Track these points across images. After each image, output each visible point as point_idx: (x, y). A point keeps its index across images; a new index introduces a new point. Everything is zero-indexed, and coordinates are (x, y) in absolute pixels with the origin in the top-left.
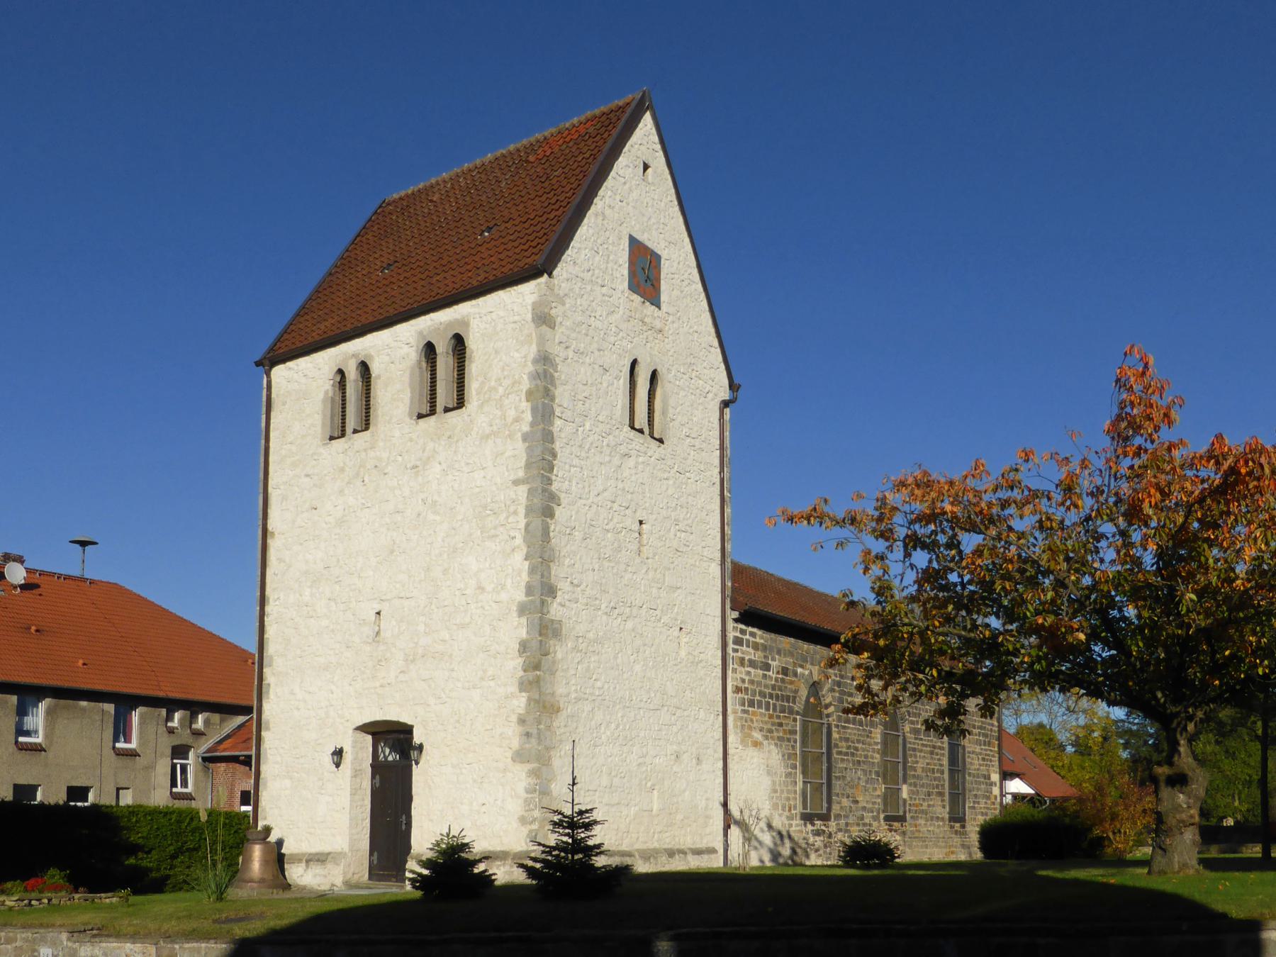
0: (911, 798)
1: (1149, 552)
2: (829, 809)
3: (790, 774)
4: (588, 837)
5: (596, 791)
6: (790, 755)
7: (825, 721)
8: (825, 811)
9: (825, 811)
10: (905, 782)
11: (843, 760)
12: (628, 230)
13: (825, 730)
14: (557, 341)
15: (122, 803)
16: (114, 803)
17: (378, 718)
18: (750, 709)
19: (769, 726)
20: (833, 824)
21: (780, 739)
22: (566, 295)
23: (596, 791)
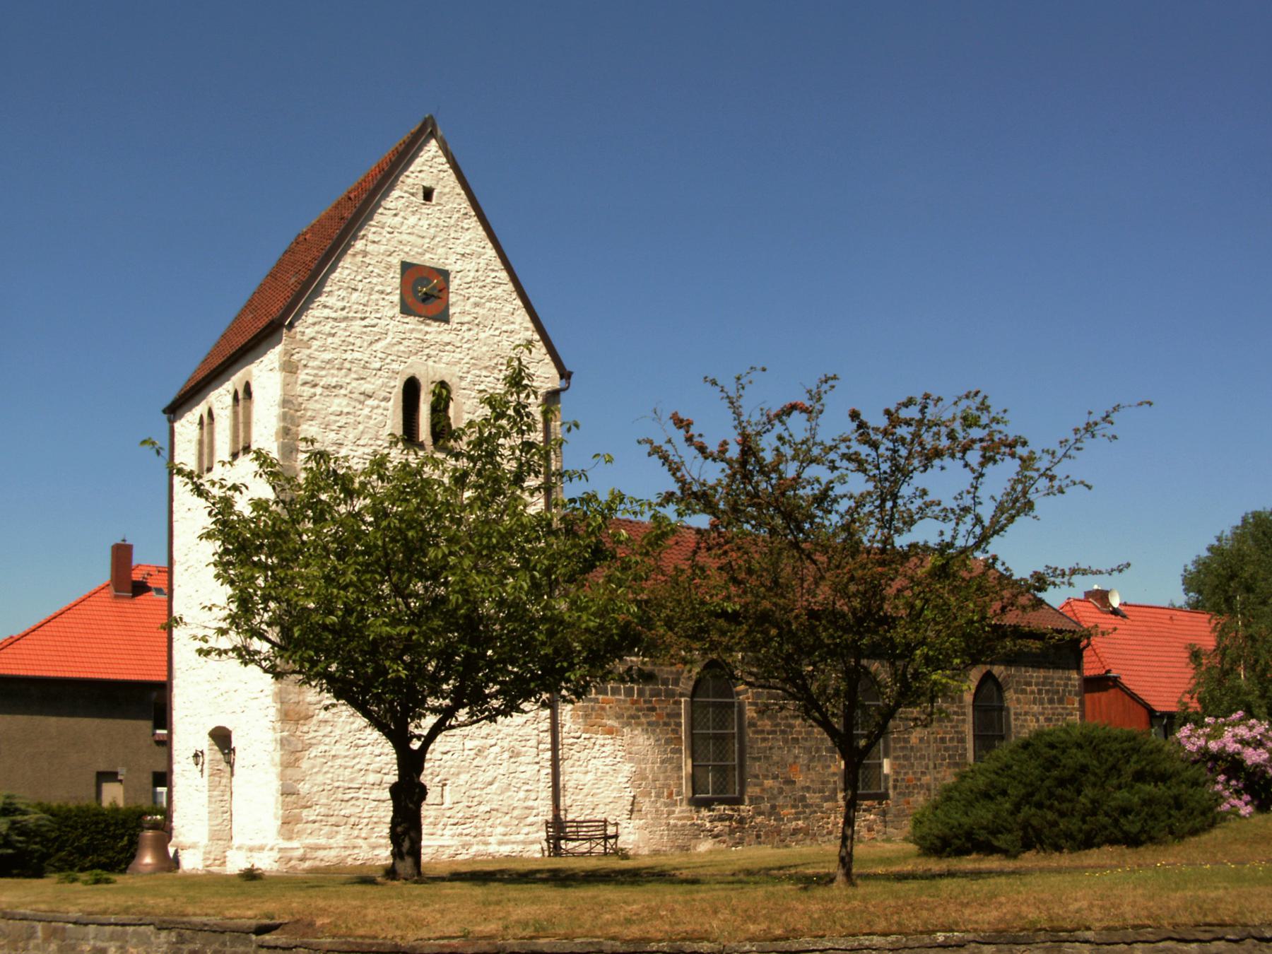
0: (897, 773)
1: (656, 670)
2: (742, 792)
3: (669, 760)
4: (202, 771)
5: (359, 788)
6: (668, 742)
7: (735, 700)
8: (737, 794)
9: (737, 794)
10: (886, 756)
11: (764, 740)
12: (425, 210)
13: (736, 709)
14: (300, 382)
15: (106, 802)
16: (94, 804)
17: (386, 830)
18: (600, 697)
19: (633, 712)
20: (746, 808)
21: (649, 724)
22: (312, 338)
23: (359, 788)
